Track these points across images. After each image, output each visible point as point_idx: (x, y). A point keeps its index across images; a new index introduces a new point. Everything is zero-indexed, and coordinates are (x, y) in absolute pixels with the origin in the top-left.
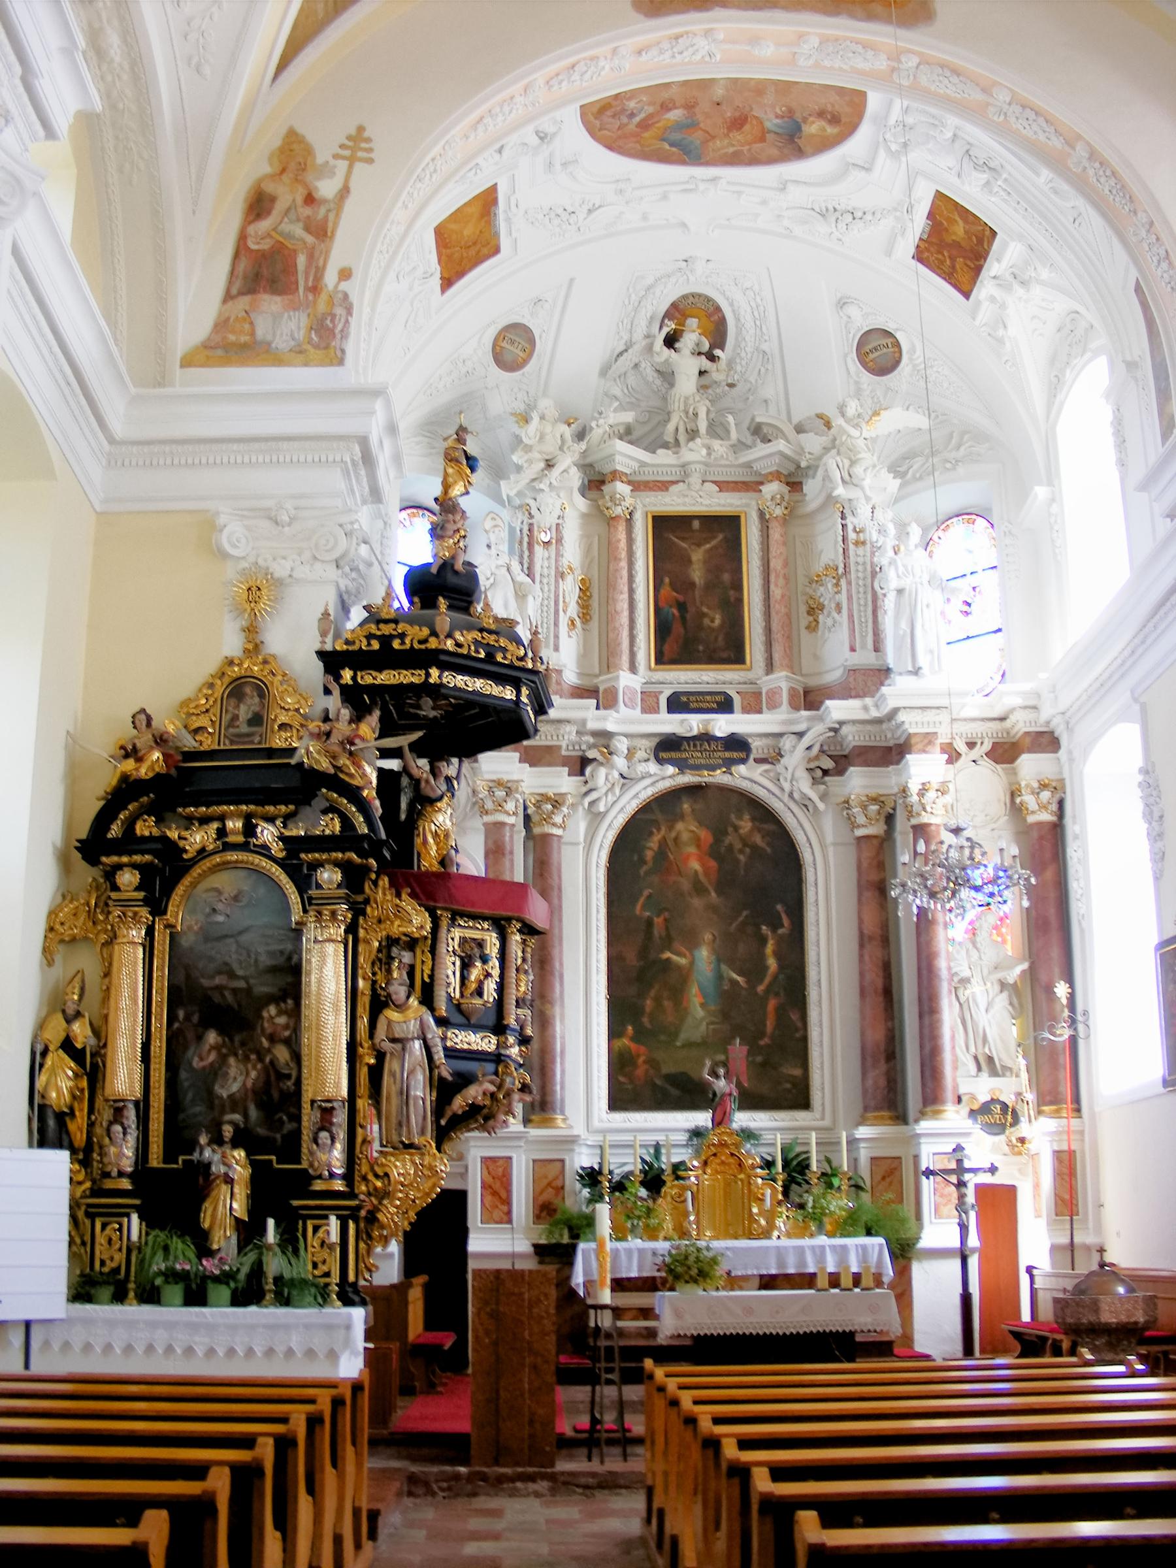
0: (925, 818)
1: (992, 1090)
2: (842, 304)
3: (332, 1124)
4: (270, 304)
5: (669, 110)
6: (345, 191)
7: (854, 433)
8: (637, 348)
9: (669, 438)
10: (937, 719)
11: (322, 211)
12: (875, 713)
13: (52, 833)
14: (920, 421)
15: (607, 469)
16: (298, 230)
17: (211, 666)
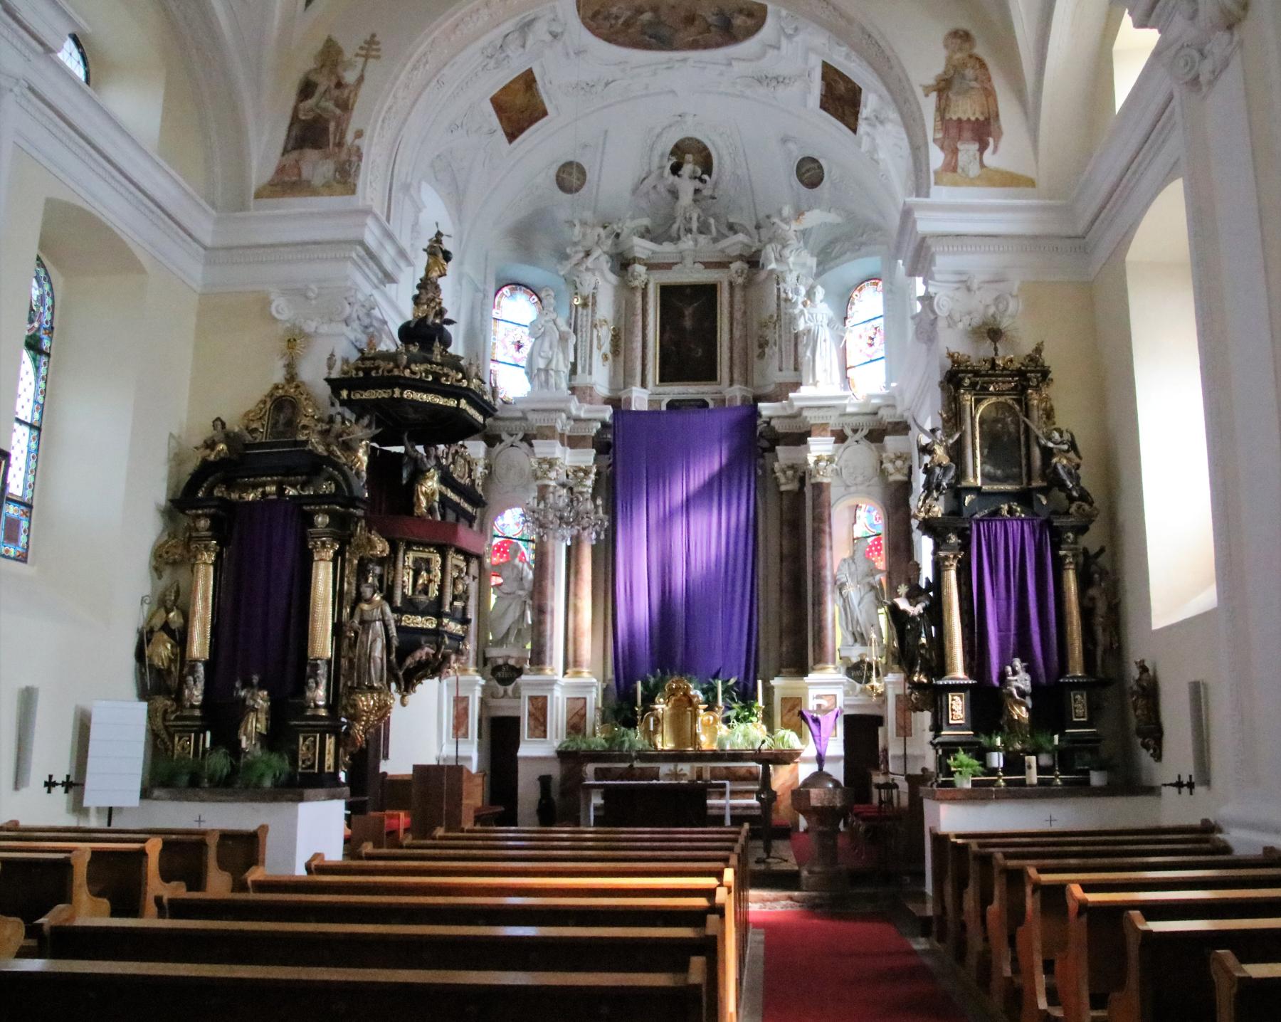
0: (819, 479)
1: (861, 655)
2: (785, 140)
3: (317, 674)
4: (311, 155)
5: (642, 13)
6: (361, 79)
7: (786, 227)
8: (653, 176)
9: (674, 234)
10: (829, 414)
11: (346, 92)
12: (789, 412)
13: (159, 493)
14: (832, 218)
15: (631, 256)
16: (330, 105)
17: (267, 388)
